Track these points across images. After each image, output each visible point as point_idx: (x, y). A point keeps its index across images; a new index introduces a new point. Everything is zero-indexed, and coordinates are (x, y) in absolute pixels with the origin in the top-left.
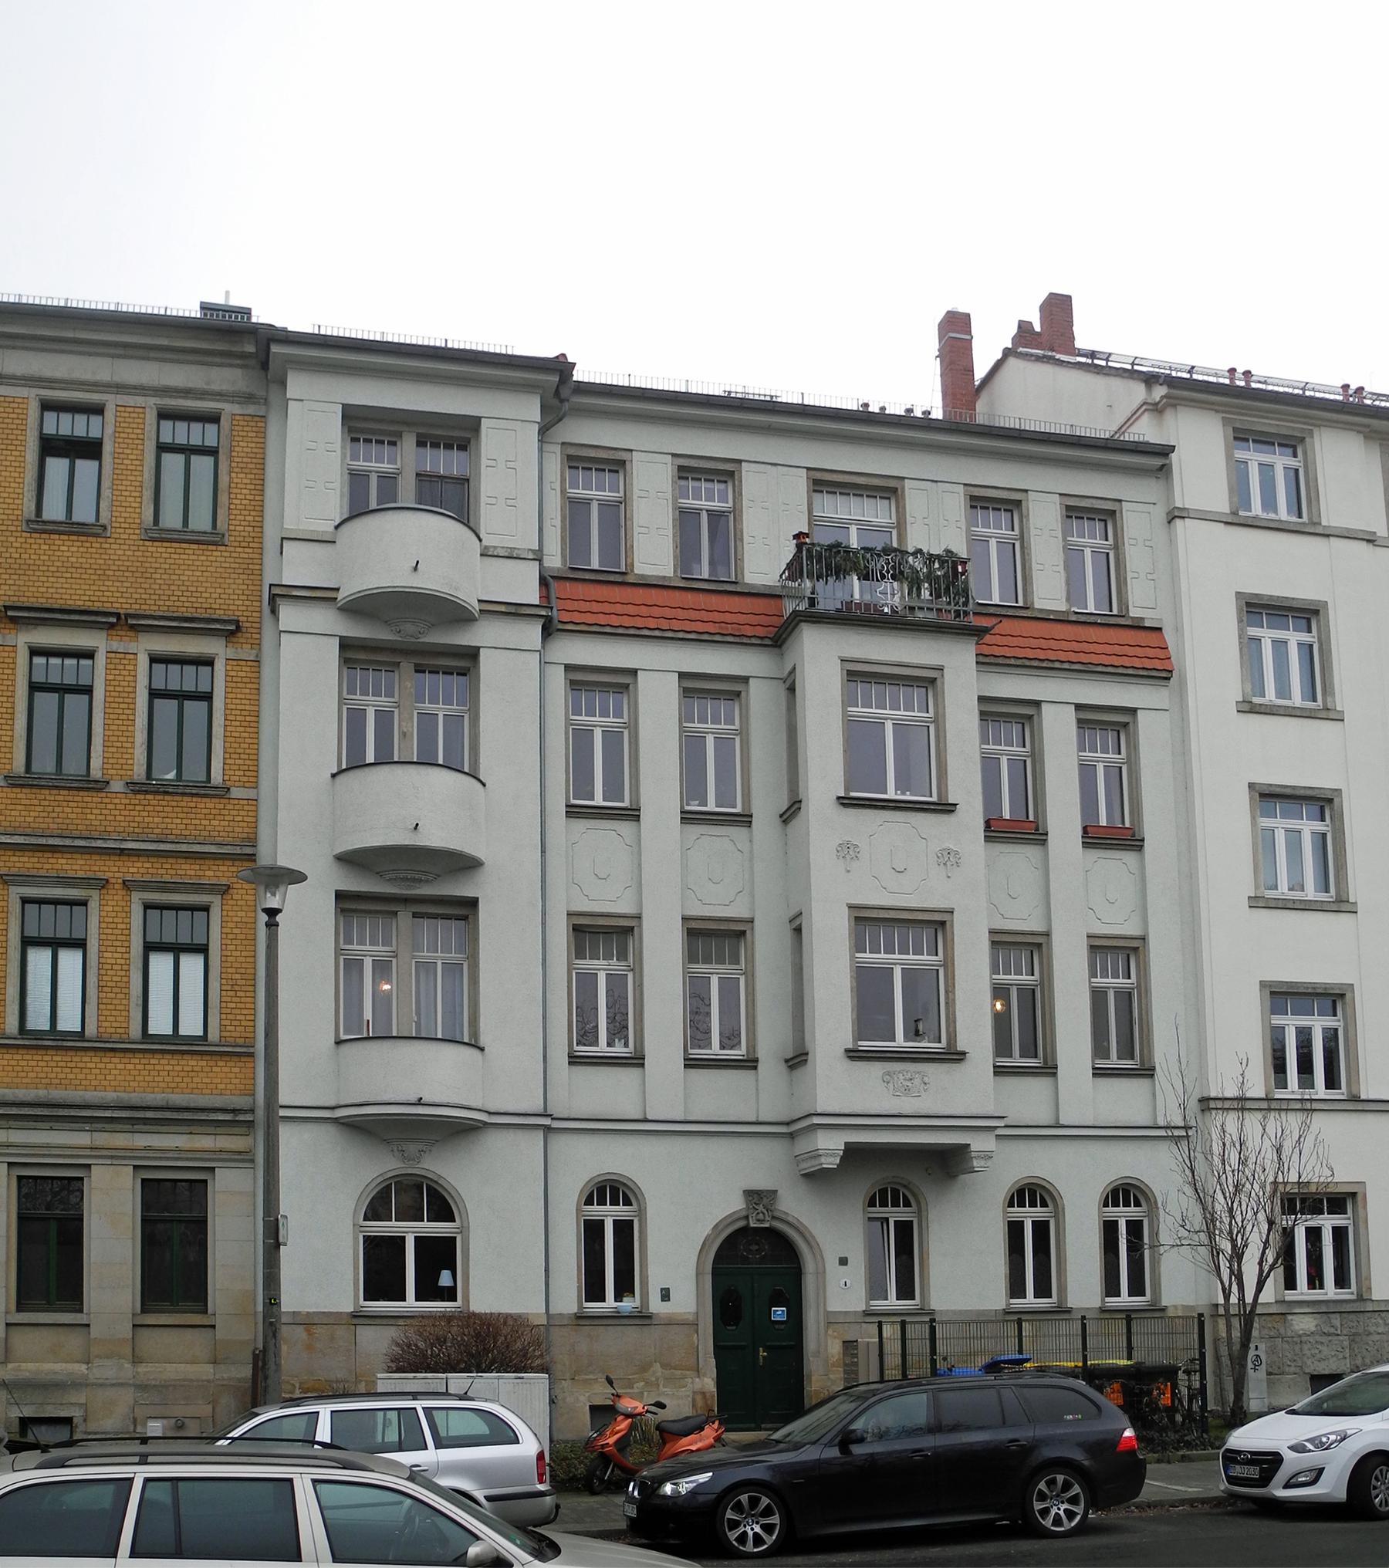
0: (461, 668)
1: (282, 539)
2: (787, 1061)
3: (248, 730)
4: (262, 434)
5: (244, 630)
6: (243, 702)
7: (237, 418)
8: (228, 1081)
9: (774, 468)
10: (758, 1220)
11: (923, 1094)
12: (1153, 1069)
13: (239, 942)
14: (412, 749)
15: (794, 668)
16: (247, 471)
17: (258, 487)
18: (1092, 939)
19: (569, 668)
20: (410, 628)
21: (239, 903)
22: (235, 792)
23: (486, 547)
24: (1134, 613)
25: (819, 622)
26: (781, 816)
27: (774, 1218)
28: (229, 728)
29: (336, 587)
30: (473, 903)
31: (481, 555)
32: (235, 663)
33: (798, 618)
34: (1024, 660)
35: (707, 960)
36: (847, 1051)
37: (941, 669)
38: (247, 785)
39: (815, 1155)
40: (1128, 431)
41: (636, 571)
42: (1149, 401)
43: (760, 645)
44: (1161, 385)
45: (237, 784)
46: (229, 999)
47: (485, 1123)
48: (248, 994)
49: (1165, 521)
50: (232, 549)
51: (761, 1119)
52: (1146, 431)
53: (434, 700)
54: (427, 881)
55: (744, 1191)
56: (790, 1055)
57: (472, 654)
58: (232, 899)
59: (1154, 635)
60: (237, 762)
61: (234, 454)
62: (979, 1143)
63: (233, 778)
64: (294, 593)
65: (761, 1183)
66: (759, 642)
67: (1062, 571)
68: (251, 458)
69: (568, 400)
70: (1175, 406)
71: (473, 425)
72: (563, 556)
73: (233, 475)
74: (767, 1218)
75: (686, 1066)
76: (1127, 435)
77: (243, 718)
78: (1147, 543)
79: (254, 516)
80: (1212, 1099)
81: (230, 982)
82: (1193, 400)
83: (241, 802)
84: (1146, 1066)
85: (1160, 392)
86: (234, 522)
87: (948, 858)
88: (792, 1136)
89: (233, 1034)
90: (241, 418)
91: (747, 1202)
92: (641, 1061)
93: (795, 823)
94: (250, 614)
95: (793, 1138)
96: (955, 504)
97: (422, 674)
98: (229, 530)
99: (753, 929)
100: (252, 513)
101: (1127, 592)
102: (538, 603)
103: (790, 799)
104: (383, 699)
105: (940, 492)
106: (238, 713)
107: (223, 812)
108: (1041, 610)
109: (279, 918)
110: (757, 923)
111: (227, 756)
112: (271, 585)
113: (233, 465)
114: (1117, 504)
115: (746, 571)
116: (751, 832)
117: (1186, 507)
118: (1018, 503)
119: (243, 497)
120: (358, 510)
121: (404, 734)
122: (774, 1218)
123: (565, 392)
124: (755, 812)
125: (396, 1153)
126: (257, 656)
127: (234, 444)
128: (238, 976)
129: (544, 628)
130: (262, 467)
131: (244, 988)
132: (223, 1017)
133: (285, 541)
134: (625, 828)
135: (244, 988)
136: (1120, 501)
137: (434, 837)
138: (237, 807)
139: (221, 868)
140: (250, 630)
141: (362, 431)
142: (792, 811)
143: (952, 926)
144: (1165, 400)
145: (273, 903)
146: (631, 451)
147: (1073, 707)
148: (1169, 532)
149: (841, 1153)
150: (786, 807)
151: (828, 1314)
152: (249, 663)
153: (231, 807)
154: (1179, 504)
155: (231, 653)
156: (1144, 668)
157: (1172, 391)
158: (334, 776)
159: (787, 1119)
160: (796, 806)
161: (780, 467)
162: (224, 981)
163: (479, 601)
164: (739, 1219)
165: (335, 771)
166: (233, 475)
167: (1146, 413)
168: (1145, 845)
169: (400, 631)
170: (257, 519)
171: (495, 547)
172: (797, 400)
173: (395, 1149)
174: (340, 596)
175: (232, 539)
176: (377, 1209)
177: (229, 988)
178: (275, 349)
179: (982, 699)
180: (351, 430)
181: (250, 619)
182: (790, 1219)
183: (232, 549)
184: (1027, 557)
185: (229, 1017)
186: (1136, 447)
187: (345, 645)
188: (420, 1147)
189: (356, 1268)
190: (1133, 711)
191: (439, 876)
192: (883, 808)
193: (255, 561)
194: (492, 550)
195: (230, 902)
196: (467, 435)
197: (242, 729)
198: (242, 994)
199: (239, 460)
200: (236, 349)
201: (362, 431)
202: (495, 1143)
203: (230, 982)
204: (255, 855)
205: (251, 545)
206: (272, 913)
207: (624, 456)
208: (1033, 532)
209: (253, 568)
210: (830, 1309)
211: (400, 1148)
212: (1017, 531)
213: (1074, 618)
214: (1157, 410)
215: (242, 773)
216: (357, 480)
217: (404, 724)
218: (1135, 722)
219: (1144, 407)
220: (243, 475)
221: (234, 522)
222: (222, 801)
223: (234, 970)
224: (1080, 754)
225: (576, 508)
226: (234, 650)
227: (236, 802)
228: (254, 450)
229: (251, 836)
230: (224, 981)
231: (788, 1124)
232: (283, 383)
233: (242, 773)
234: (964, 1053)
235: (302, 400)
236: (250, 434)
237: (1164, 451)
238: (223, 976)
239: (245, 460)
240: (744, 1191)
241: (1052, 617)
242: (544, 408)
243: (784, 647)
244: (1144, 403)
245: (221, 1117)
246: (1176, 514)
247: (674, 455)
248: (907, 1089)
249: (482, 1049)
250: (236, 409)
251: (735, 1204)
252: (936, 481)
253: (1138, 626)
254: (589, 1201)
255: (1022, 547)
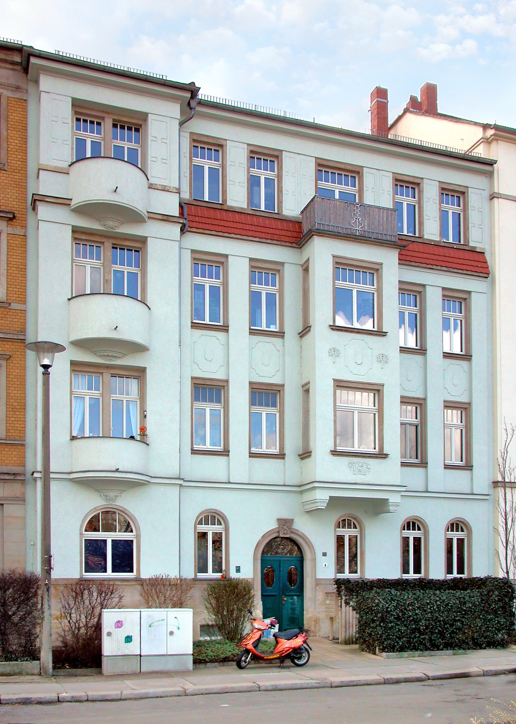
0: (138, 248)
1: (39, 169)
2: (299, 455)
3: (20, 272)
4: (25, 110)
5: (17, 218)
6: (18, 257)
7: (10, 99)
8: (11, 459)
9: (299, 156)
10: (284, 533)
11: (367, 473)
12: (472, 466)
13: (16, 386)
14: (111, 289)
15: (309, 259)
16: (17, 130)
17: (24, 140)
18: (446, 403)
19: (193, 251)
20: (110, 223)
21: (16, 365)
22: (14, 306)
23: (151, 184)
24: (472, 244)
25: (322, 236)
26: (299, 334)
27: (292, 532)
28: (9, 271)
29: (70, 198)
30: (143, 370)
31: (148, 188)
32: (12, 236)
33: (313, 233)
34: (419, 264)
35: (261, 405)
36: (331, 451)
37: (381, 264)
38: (20, 302)
39: (314, 501)
40: (473, 151)
41: (228, 204)
42: (484, 137)
43: (290, 247)
44: (491, 129)
45: (14, 301)
46: (11, 416)
47: (149, 482)
48: (22, 413)
49: (489, 199)
50: (10, 173)
51: (286, 484)
52: (481, 152)
53: (122, 264)
54: (120, 357)
55: (277, 519)
56: (301, 453)
57: (143, 240)
58: (12, 363)
59: (480, 255)
60: (14, 290)
61: (9, 119)
62: (393, 499)
63: (12, 298)
64: (47, 200)
65: (285, 515)
66: (290, 245)
67: (438, 221)
68: (20, 123)
69: (195, 109)
70: (497, 140)
71: (144, 116)
72: (190, 193)
73: (9, 131)
74: (288, 532)
75: (250, 456)
76: (472, 153)
77: (17, 266)
78: (480, 210)
79: (22, 156)
80: (499, 482)
81: (11, 407)
82: (508, 138)
83: (17, 311)
84: (469, 465)
85: (490, 132)
86: (10, 158)
87: (383, 359)
88: (301, 492)
89: (14, 434)
90: (13, 99)
91: (279, 524)
92: (227, 453)
93: (307, 338)
94: (20, 210)
95: (301, 493)
96: (388, 183)
97: (116, 250)
98: (7, 162)
99: (284, 390)
100: (21, 154)
101: (469, 234)
102: (178, 216)
103: (304, 325)
104: (95, 261)
105: (381, 175)
106: (15, 263)
107: (7, 316)
108: (427, 240)
109: (50, 370)
110: (286, 387)
111: (9, 286)
112: (33, 194)
113: (9, 126)
114: (466, 188)
115: (284, 209)
116: (228, 335)
117: (500, 192)
118: (418, 184)
119: (15, 144)
120: (81, 158)
121: (107, 281)
122: (292, 532)
123: (193, 103)
124: (286, 330)
125: (103, 497)
126: (25, 233)
127: (9, 114)
128: (16, 404)
129: (182, 230)
130: (25, 128)
131: (19, 410)
132: (8, 425)
133: (40, 171)
134: (221, 335)
135: (19, 410)
136: (468, 187)
137: (125, 334)
138: (14, 314)
139: (6, 346)
140: (21, 219)
141: (81, 114)
142: (306, 330)
143: (383, 392)
144: (492, 137)
145: (46, 362)
146: (226, 140)
147: (441, 288)
148: (491, 206)
149: (327, 501)
150: (301, 330)
151: (317, 580)
152: (21, 237)
153: (11, 314)
154: (496, 191)
155: (10, 230)
156: (476, 272)
157: (497, 132)
158: (69, 300)
159: (299, 484)
160: (308, 329)
161: (301, 156)
162: (8, 406)
163: (148, 212)
164: (275, 533)
165: (70, 297)
166: (9, 131)
167: (482, 144)
168: (427, 353)
169: (105, 225)
170: (23, 157)
171: (156, 185)
172: (311, 120)
173: (102, 495)
174: (73, 203)
175: (10, 167)
176: (92, 526)
177: (11, 410)
178: (33, 60)
179: (400, 282)
180: (76, 113)
181: (20, 213)
182: (300, 533)
183: (10, 173)
184: (421, 213)
185: (11, 425)
186: (478, 160)
187: (75, 230)
188: (116, 494)
189: (81, 555)
190: (469, 293)
191: (126, 355)
192: (352, 332)
193: (23, 181)
194: (154, 186)
195: (11, 365)
196: (140, 123)
197: (17, 272)
198: (18, 413)
199: (13, 123)
200: (8, 58)
201: (81, 114)
202: (155, 492)
203: (11, 407)
204: (24, 340)
205: (20, 172)
206: (46, 367)
207: (223, 142)
208: (425, 200)
209: (22, 185)
210: (317, 577)
211: (105, 494)
212: (417, 199)
213: (443, 245)
214: (488, 142)
215: (17, 296)
216: (80, 144)
217: (106, 275)
218: (470, 297)
219: (482, 140)
220: (15, 132)
221: (10, 158)
222: (6, 310)
223: (14, 401)
224: (443, 312)
225: (197, 172)
226: (12, 229)
227: (14, 311)
228: (21, 119)
229: (23, 330)
230: (8, 406)
231: (300, 486)
232: (36, 82)
233: (17, 296)
234: (387, 455)
235: (49, 93)
236: (18, 109)
237: (491, 163)
238: (8, 403)
239: (16, 124)
240: (277, 519)
241: (432, 243)
242: (182, 112)
243: (303, 248)
244: (482, 138)
245: (7, 477)
246: (495, 196)
247: (248, 145)
248: (360, 471)
249: (148, 445)
250: (10, 94)
251: (273, 525)
252: (379, 170)
253: (473, 251)
254: (200, 523)
255: (420, 207)
